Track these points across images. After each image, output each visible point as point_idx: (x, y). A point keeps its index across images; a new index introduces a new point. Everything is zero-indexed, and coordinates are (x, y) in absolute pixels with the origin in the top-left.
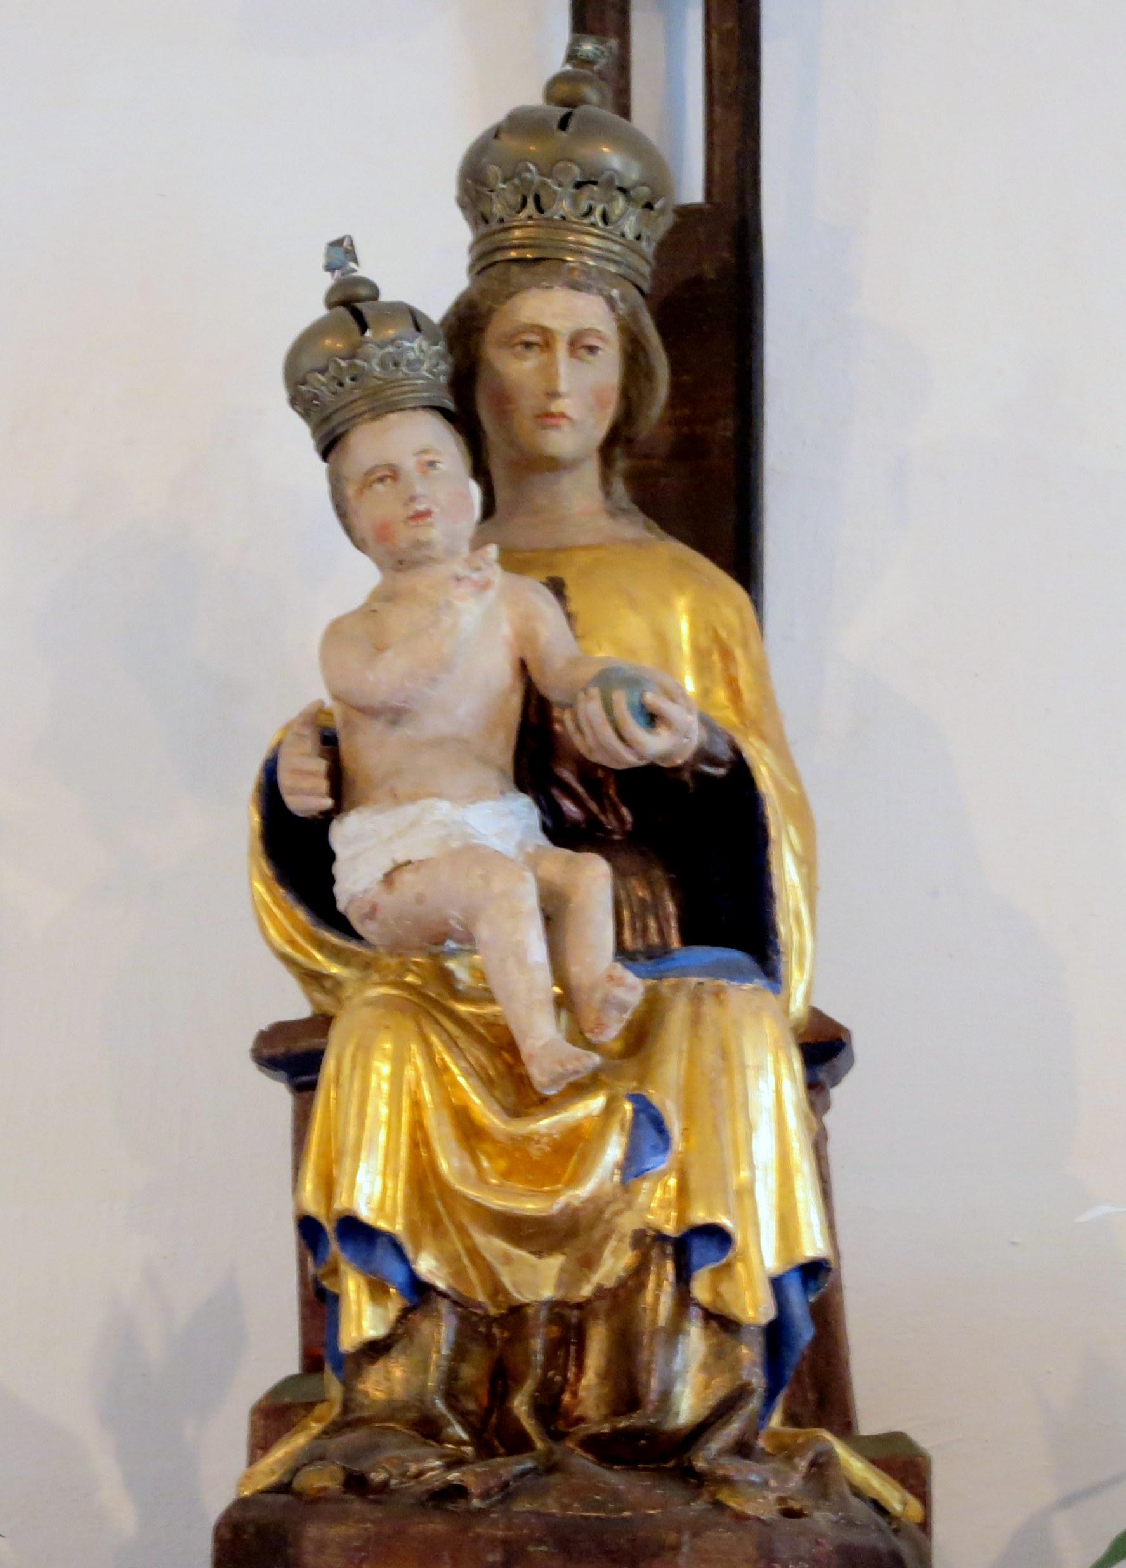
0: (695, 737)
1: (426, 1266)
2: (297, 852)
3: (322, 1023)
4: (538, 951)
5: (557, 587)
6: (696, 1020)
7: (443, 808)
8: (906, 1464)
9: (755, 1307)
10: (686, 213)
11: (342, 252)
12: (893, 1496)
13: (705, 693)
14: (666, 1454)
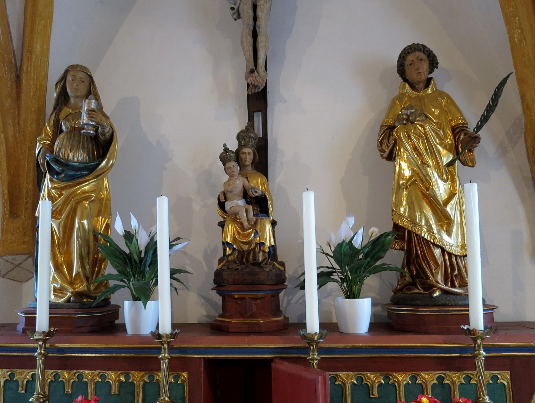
0: (261, 193)
1: (235, 246)
2: (222, 205)
3: (224, 222)
4: (245, 215)
5: (247, 178)
6: (261, 222)
7: (236, 201)
8: (283, 264)
9: (267, 250)
10: (260, 138)
11: (225, 145)
12: (281, 268)
13: (262, 188)
14: (258, 264)
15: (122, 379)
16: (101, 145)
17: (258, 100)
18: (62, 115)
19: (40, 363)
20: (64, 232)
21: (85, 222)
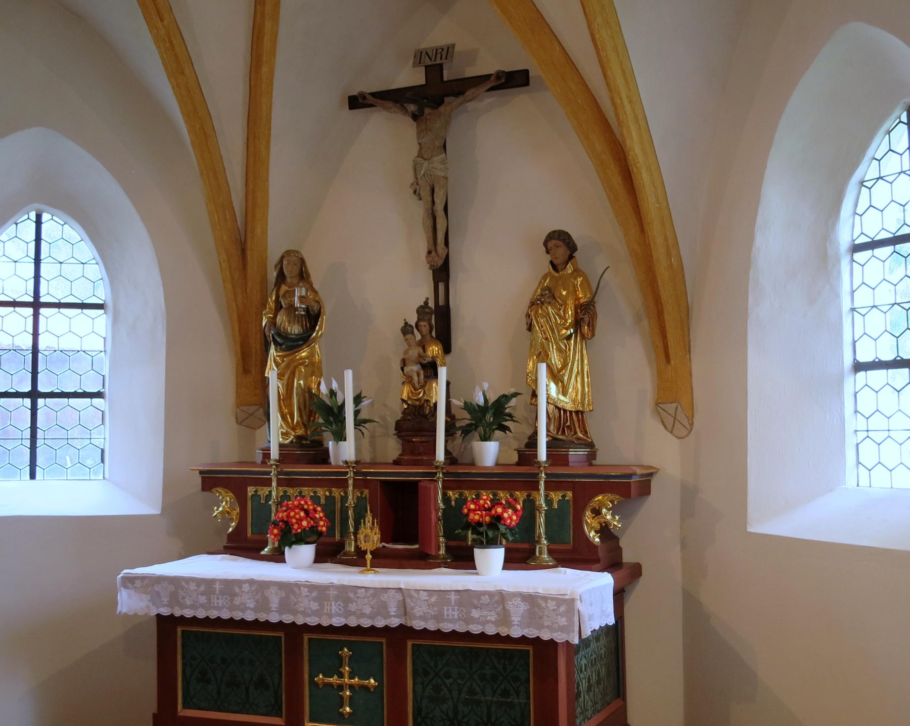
14: (425, 416)
15: (327, 493)
16: (312, 318)
17: (442, 273)
18: (281, 292)
19: (274, 484)
20: (287, 390)
21: (302, 382)
